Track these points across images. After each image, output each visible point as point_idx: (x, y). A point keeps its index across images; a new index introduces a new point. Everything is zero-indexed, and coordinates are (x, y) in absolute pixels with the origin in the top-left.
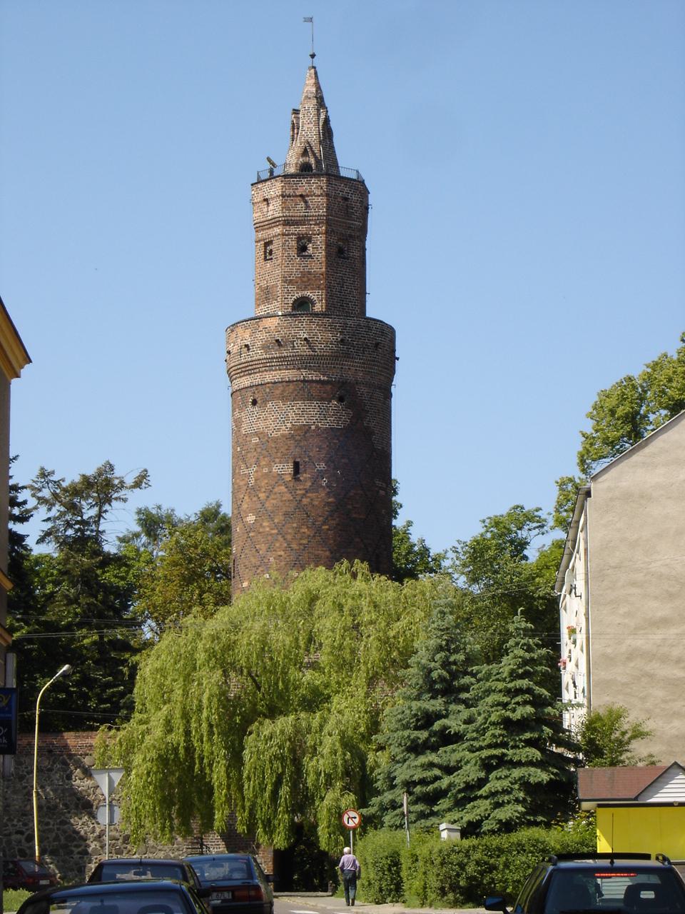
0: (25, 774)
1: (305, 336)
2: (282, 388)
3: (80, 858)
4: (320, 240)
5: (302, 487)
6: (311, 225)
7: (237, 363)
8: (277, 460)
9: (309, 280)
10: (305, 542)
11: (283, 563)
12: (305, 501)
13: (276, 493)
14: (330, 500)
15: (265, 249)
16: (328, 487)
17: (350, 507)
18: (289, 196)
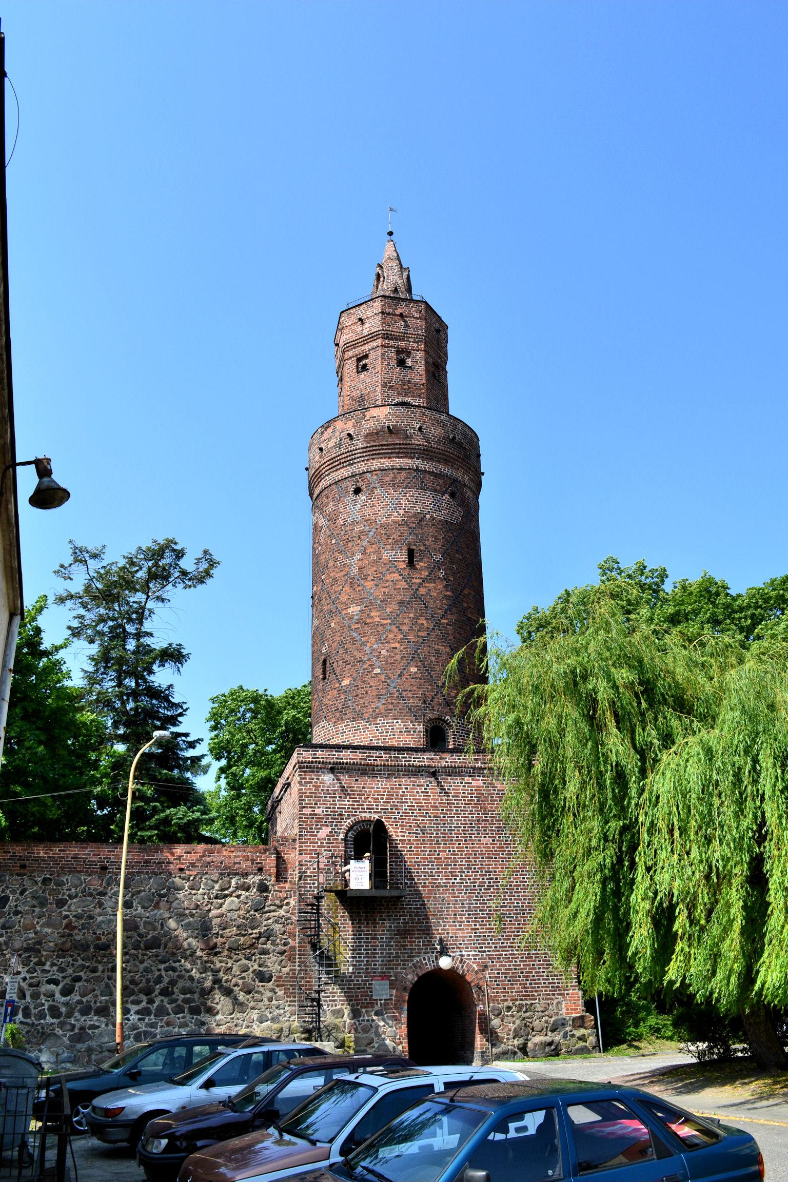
0: (66, 897)
2: (393, 475)
3: (139, 1019)
4: (420, 356)
5: (418, 576)
6: (410, 342)
7: (329, 458)
8: (389, 547)
9: (409, 388)
10: (424, 634)
11: (398, 657)
12: (423, 591)
14: (448, 593)
15: (358, 364)
16: (445, 579)
17: (465, 605)
18: (389, 314)
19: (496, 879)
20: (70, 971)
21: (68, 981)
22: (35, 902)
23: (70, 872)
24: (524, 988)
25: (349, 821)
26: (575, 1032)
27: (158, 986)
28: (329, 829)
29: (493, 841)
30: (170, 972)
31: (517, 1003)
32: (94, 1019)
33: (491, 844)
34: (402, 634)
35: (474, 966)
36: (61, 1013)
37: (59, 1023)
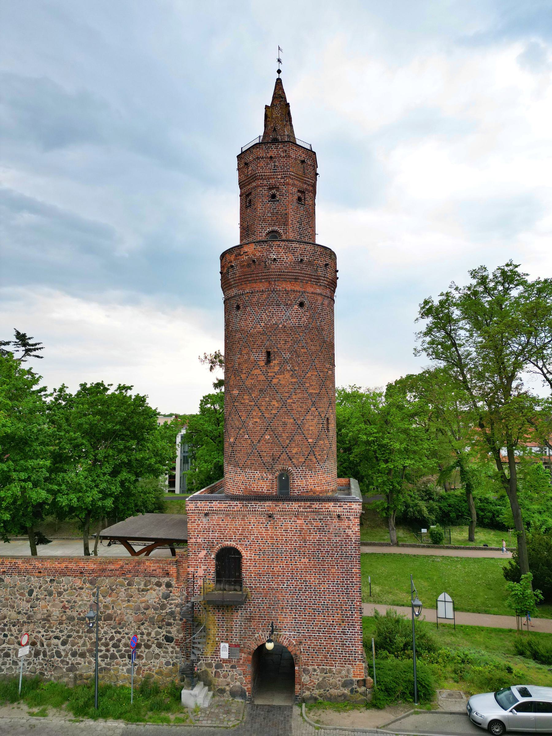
1: (274, 257)
13: (253, 375)
16: (292, 370)
19: (310, 586)
20: (66, 632)
21: (64, 637)
22: (46, 593)
23: (64, 576)
24: (326, 658)
25: (217, 547)
26: (358, 689)
27: (111, 642)
28: (205, 552)
29: (309, 560)
30: (118, 634)
31: (320, 667)
32: (79, 659)
33: (308, 563)
34: (261, 412)
35: (294, 641)
36: (62, 655)
37: (61, 661)
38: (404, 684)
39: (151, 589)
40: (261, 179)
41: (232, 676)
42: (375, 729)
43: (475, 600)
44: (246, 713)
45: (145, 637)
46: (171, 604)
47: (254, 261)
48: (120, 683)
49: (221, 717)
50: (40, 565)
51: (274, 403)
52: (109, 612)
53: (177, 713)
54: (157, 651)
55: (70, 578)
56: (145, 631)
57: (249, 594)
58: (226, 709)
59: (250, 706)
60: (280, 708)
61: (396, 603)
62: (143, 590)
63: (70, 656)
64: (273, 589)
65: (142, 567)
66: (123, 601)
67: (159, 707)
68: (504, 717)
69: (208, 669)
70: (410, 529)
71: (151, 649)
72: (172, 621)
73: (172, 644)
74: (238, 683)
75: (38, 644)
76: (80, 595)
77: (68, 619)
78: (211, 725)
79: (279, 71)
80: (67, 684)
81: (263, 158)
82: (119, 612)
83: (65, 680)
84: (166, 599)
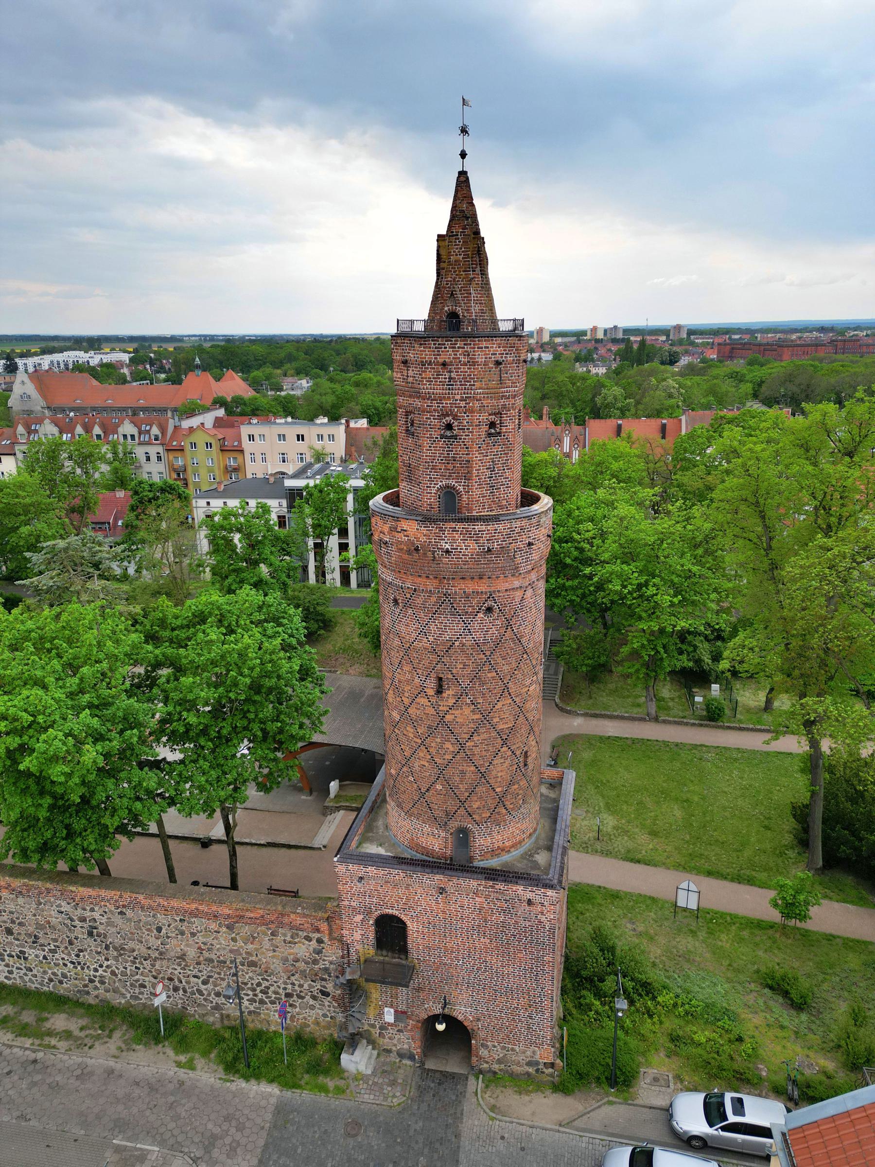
1: (447, 546)
20: (205, 972)
21: (205, 977)
26: (545, 1070)
28: (362, 917)
38: (600, 1068)
39: (299, 942)
40: (428, 399)
41: (399, 1039)
42: (557, 1127)
43: (739, 854)
44: (414, 1083)
45: (296, 988)
46: (324, 960)
47: (417, 549)
48: (273, 1028)
49: (385, 1091)
50: (166, 903)
51: (448, 745)
52: (254, 958)
53: (336, 1079)
54: (312, 1002)
55: (203, 920)
56: (296, 982)
57: (417, 965)
58: (392, 1078)
59: (419, 1072)
60: (454, 1078)
61: (630, 856)
62: (290, 943)
63: (213, 995)
64: (445, 964)
65: (286, 920)
66: (268, 950)
67: (317, 1068)
68: (707, 1135)
69: (371, 1029)
70: (683, 680)
71: (305, 1000)
72: (326, 976)
73: (329, 999)
74: (406, 1046)
75: (176, 980)
76: (217, 938)
77: (206, 960)
78: (374, 1102)
79: (463, 155)
80: (213, 1024)
81: (430, 364)
82: (264, 960)
83: (211, 1019)
84: (318, 954)
